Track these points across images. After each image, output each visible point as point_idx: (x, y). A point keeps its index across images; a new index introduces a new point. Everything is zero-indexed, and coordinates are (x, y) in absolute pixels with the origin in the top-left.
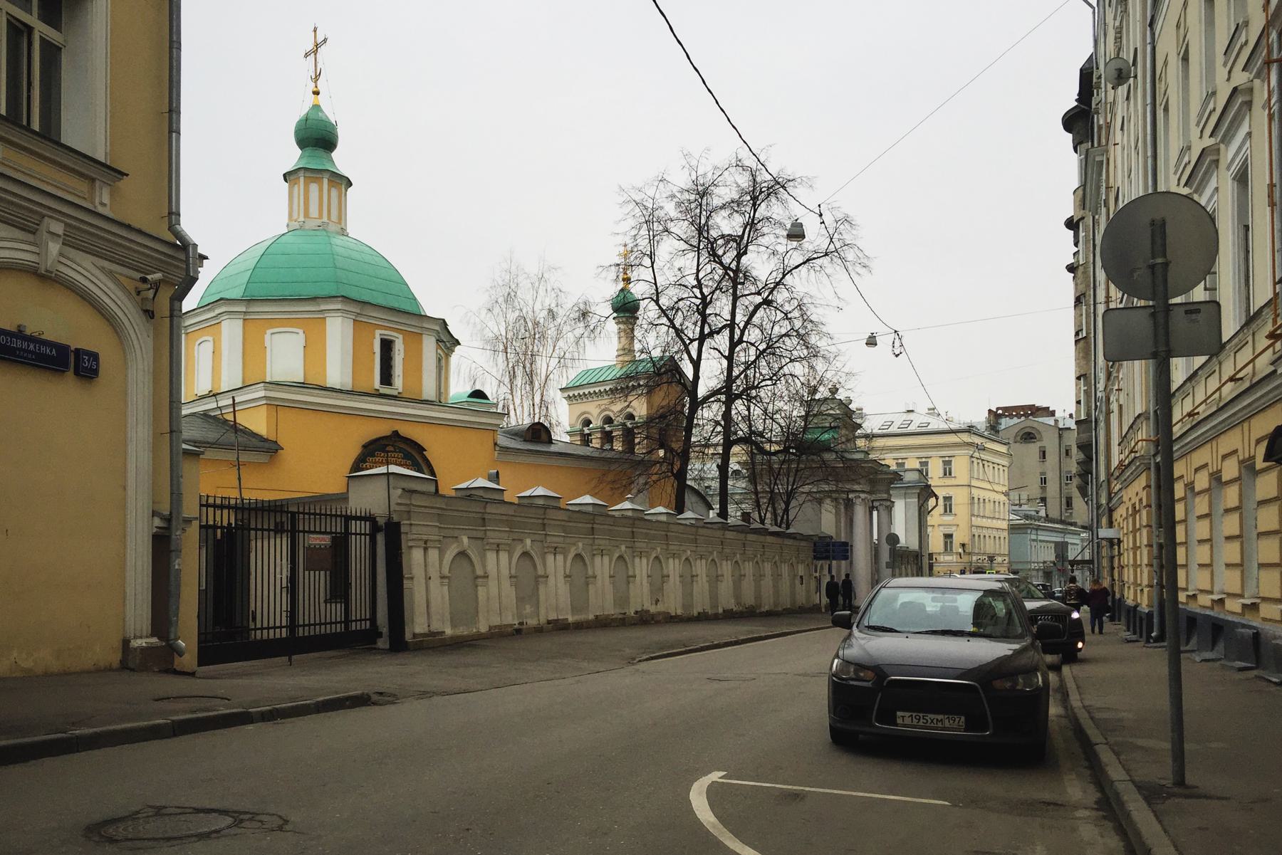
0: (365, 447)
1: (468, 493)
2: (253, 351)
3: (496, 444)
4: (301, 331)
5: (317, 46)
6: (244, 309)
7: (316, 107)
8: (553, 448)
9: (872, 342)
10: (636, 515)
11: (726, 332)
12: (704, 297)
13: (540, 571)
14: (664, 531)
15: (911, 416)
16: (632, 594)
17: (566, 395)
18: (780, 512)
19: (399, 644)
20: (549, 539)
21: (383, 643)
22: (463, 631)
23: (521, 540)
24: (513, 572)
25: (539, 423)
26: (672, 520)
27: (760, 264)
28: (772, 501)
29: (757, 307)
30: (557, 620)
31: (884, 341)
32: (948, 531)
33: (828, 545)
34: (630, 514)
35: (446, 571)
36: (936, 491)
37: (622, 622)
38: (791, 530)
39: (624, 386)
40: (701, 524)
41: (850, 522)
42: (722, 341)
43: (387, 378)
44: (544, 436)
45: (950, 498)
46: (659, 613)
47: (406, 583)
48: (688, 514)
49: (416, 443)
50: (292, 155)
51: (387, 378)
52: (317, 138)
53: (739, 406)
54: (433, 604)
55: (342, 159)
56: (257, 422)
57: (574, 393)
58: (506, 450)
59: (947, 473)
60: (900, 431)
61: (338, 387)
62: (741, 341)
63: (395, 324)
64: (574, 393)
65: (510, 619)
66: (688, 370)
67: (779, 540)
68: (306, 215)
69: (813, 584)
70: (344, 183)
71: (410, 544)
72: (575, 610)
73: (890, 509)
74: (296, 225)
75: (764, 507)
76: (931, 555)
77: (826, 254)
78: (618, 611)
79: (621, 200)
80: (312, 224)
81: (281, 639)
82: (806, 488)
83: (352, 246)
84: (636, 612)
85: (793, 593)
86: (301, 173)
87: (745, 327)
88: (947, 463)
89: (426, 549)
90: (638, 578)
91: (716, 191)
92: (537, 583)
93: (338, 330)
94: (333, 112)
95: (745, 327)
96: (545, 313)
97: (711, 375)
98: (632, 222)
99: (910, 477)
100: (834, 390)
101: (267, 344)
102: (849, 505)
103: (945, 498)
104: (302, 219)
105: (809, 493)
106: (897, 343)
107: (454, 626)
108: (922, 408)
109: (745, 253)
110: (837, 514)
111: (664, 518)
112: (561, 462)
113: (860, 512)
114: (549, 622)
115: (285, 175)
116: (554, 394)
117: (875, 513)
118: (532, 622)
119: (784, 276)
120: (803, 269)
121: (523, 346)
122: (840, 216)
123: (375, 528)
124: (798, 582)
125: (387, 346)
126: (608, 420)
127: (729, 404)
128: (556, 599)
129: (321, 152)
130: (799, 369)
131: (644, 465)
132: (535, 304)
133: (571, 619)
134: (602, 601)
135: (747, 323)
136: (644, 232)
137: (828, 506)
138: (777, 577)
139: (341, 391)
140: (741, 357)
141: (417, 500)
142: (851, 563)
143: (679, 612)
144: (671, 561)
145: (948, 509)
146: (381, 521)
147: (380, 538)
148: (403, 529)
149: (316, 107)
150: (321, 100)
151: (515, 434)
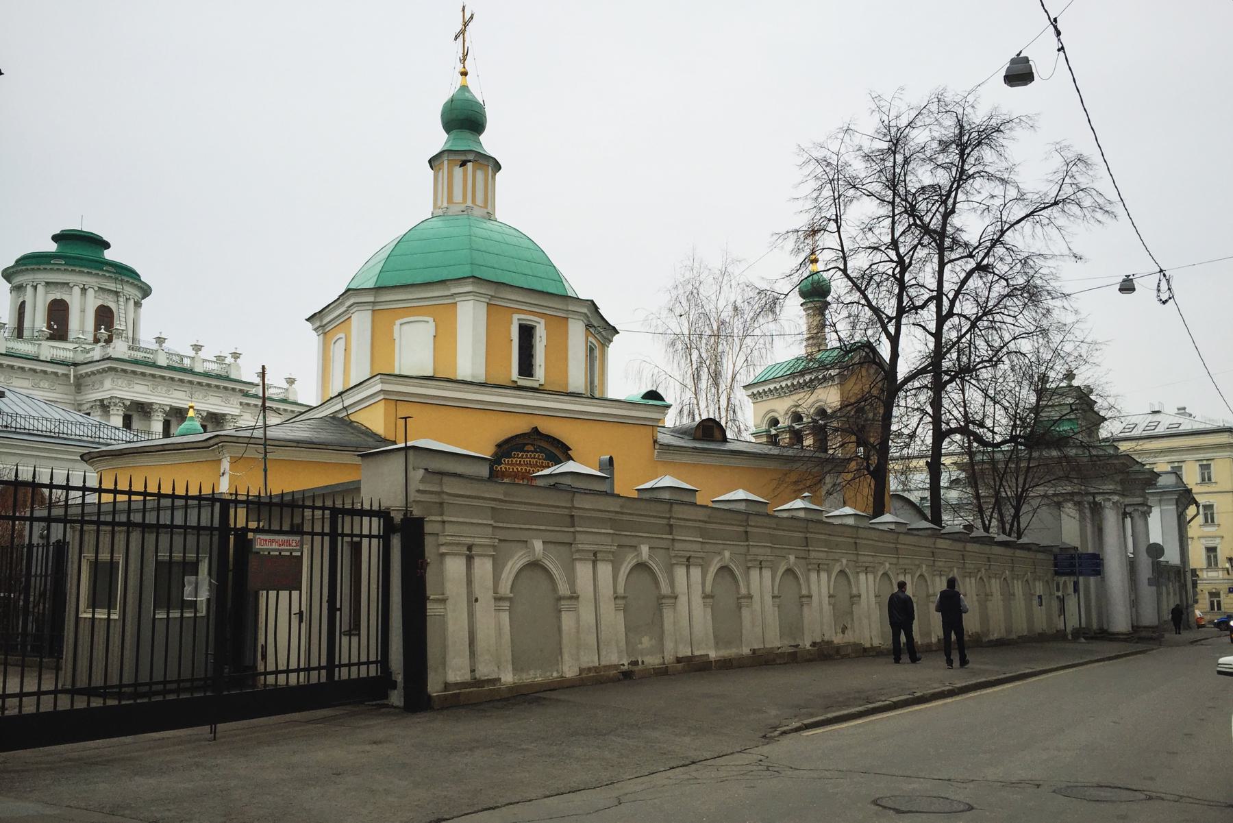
0: (499, 446)
1: (552, 481)
2: (381, 342)
3: (655, 442)
4: (430, 319)
5: (466, 25)
6: (371, 299)
7: (464, 88)
8: (729, 446)
9: (1127, 287)
10: (810, 516)
11: (932, 306)
12: (901, 258)
13: (665, 589)
14: (852, 536)
15: (1157, 417)
16: (806, 621)
17: (750, 392)
18: (1008, 519)
19: (418, 701)
20: (678, 546)
21: (396, 698)
22: (534, 676)
23: (635, 547)
24: (621, 591)
25: (709, 420)
26: (865, 523)
27: (970, 224)
28: (998, 504)
29: (969, 275)
30: (693, 657)
31: (1146, 286)
32: (1211, 544)
33: (1072, 557)
34: (802, 514)
35: (505, 589)
36: (1198, 498)
37: (793, 659)
38: (1024, 540)
39: (806, 374)
40: (903, 529)
41: (1099, 531)
42: (929, 316)
43: (526, 367)
44: (717, 434)
45: (1211, 506)
46: (847, 645)
47: (432, 608)
48: (887, 518)
49: (559, 441)
50: (439, 139)
51: (526, 367)
52: (465, 119)
53: (952, 393)
54: (480, 636)
55: (489, 142)
56: (375, 420)
57: (759, 390)
58: (666, 447)
59: (1206, 478)
60: (1145, 434)
61: (469, 379)
62: (951, 314)
63: (536, 308)
64: (759, 390)
65: (615, 657)
66: (885, 351)
67: (1009, 552)
68: (450, 200)
69: (1055, 604)
70: (491, 164)
71: (443, 550)
72: (718, 642)
73: (1146, 515)
74: (439, 212)
75: (988, 513)
76: (1194, 571)
77: (1056, 203)
78: (787, 642)
79: (801, 160)
80: (455, 209)
81: (319, 684)
82: (1040, 490)
83: (499, 229)
84: (814, 644)
85: (1030, 619)
86: (445, 157)
87: (956, 297)
88: (1205, 468)
89: (470, 559)
90: (815, 599)
91: (913, 133)
92: (660, 607)
93: (470, 316)
94: (480, 91)
95: (956, 297)
96: (730, 308)
97: (914, 348)
98: (814, 184)
99: (1166, 481)
100: (1070, 376)
101: (396, 335)
102: (1097, 509)
103: (1205, 507)
104: (445, 204)
105: (1045, 496)
106: (1164, 286)
107: (516, 669)
108: (1170, 409)
109: (953, 211)
110: (1082, 519)
111: (851, 521)
112: (735, 462)
113: (1111, 518)
114: (679, 660)
115: (430, 161)
116: (740, 396)
117: (1128, 521)
118: (652, 661)
119: (1003, 232)
120: (1027, 225)
121: (705, 344)
122: (1070, 155)
123: (389, 526)
124: (1035, 602)
125: (527, 333)
126: (797, 417)
127: (938, 388)
128: (690, 625)
129: (467, 134)
130: (1025, 345)
131: (838, 465)
132: (721, 301)
133: (713, 655)
134: (762, 627)
135: (958, 293)
136: (827, 192)
137: (1070, 509)
138: (1008, 596)
139: (472, 383)
140: (950, 335)
141: (451, 486)
142: (1103, 579)
143: (876, 643)
144: (862, 577)
145: (1209, 519)
146: (398, 517)
147: (396, 541)
148: (428, 528)
149: (464, 88)
150: (470, 81)
151: (681, 432)
